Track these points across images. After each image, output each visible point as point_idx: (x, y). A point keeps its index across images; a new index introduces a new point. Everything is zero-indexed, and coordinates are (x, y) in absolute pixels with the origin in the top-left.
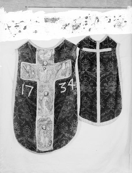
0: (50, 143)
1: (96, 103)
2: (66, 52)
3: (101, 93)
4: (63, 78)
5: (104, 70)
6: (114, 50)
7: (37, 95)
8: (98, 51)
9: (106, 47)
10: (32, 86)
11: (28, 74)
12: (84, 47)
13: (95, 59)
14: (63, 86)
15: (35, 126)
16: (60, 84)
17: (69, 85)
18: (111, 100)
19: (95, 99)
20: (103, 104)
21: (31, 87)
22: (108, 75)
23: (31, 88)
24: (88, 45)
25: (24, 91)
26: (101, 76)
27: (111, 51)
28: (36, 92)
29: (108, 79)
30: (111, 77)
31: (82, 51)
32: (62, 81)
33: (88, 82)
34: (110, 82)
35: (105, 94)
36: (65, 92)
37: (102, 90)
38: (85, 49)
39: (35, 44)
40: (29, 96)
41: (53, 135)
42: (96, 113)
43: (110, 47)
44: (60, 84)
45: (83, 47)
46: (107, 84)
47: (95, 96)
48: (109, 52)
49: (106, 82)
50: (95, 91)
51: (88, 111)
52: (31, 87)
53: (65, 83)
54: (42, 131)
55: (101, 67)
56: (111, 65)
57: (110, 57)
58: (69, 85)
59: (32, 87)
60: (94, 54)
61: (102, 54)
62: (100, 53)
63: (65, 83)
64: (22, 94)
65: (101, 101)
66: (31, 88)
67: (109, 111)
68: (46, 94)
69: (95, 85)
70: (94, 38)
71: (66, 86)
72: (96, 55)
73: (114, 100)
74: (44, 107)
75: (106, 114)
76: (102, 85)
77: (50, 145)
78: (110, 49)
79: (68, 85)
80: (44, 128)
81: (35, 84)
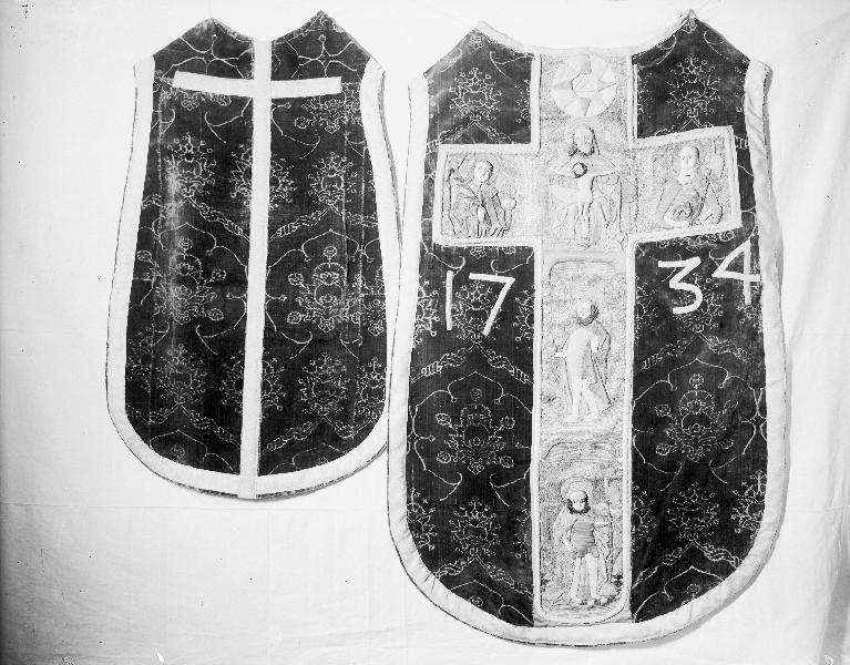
0: (610, 589)
1: (240, 384)
2: (699, 86)
3: (268, 329)
4: (682, 230)
5: (295, 200)
6: (351, 93)
7: (531, 321)
8: (262, 90)
9: (315, 72)
10: (507, 275)
11: (481, 211)
12: (183, 69)
13: (243, 133)
14: (687, 279)
15: (528, 494)
16: (661, 264)
17: (721, 273)
18: (329, 367)
19: (237, 360)
20: (275, 388)
21: (501, 279)
22: (317, 230)
23: (497, 287)
24: (205, 56)
25: (453, 312)
26: (272, 231)
27: (339, 97)
28: (531, 303)
29: (315, 250)
30: (329, 239)
31: (168, 88)
32: (678, 249)
33: (197, 265)
34: (325, 269)
35: (294, 330)
36: (695, 313)
37: (274, 310)
38: (185, 81)
39: (517, 39)
40: (486, 332)
41: (626, 542)
42: (239, 440)
43: (334, 71)
44: (661, 264)
45: (175, 68)
46: (308, 280)
47: (238, 340)
48: (327, 97)
49: (296, 264)
50: (237, 313)
51: (191, 430)
52: (501, 279)
53: (695, 262)
54: (566, 518)
55: (274, 182)
56: (332, 172)
57: (336, 126)
58: (721, 273)
59: (509, 281)
60: (241, 105)
61: (286, 112)
62: (273, 100)
63: (695, 262)
64: (449, 328)
65: (269, 370)
66: (497, 287)
67: (310, 427)
68: (586, 314)
69: (238, 281)
70: (236, 25)
71: (703, 275)
72: (249, 114)
73: (344, 368)
74: (578, 385)
75: (292, 443)
76: (275, 283)
77: (611, 599)
78: (331, 85)
79: (716, 274)
80: (578, 506)
81: (520, 264)
